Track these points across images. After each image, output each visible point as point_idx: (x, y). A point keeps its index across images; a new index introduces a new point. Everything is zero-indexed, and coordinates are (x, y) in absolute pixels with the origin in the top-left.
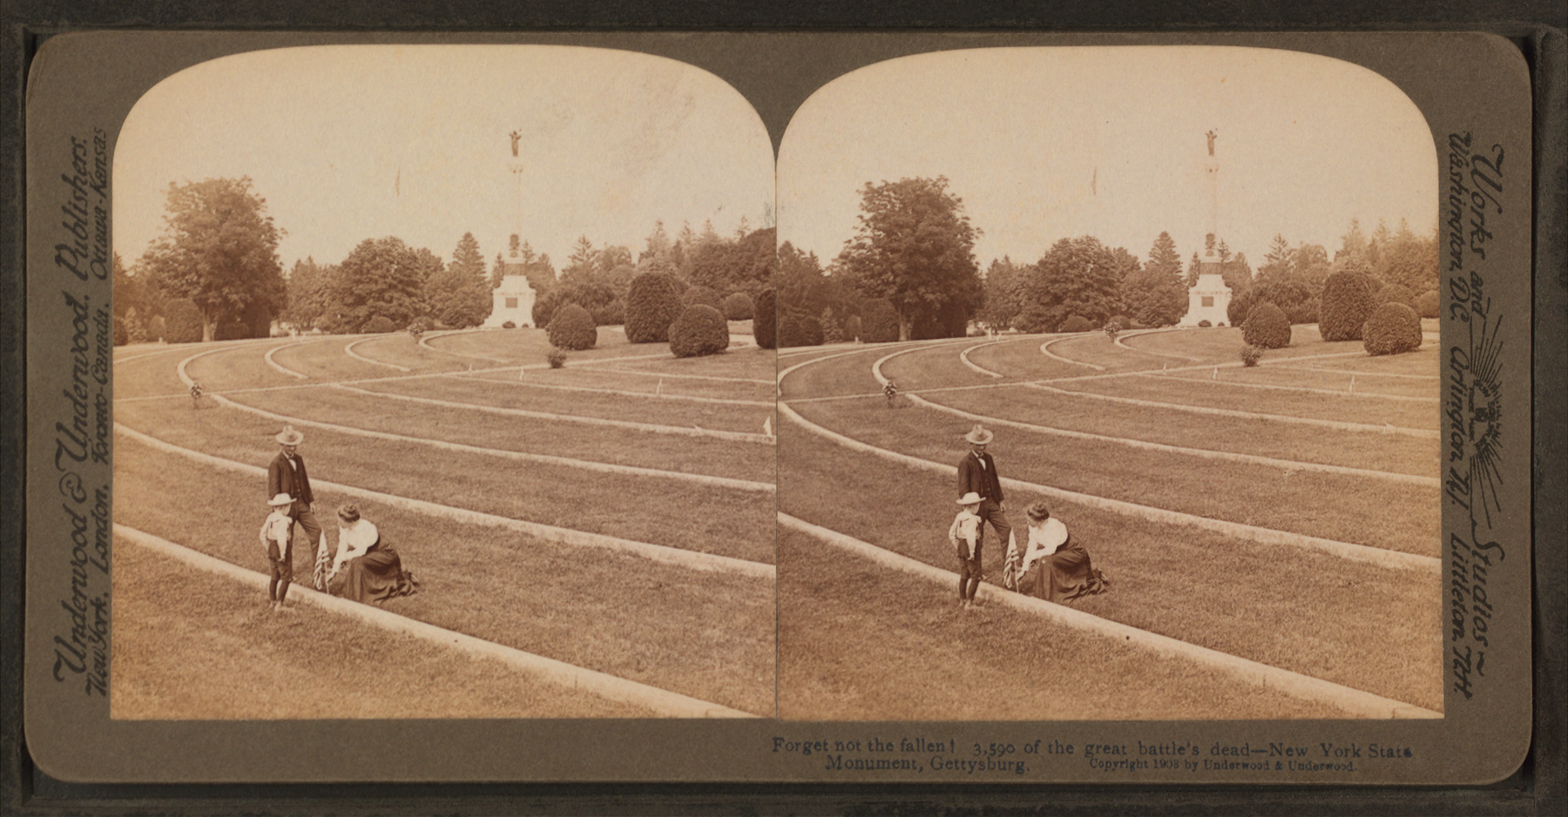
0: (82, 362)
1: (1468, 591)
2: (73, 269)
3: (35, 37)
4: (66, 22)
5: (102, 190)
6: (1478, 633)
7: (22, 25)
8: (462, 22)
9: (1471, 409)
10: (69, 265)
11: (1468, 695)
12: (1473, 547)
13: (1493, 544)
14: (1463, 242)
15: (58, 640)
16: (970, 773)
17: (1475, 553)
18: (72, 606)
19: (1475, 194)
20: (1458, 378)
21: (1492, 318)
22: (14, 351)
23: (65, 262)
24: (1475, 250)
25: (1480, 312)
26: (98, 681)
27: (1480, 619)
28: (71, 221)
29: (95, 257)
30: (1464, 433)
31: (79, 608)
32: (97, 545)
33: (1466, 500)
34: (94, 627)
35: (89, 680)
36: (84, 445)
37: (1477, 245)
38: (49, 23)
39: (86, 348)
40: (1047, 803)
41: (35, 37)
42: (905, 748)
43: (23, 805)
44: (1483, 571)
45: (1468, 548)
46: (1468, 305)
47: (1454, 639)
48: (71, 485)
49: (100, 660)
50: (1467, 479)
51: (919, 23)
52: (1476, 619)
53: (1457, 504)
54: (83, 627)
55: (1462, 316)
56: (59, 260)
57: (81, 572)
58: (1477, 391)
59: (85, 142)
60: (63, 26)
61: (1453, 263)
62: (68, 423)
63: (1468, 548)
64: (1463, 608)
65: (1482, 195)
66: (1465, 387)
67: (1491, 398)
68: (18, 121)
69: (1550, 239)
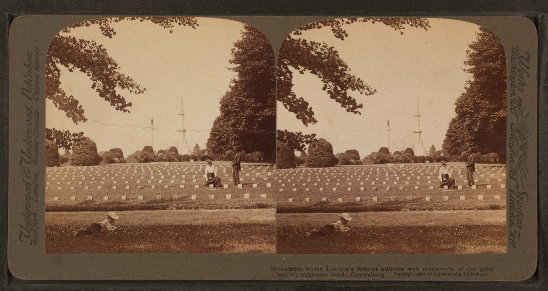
0: (30, 130)
1: (515, 210)
2: (27, 97)
3: (12, 17)
4: (23, 11)
5: (38, 69)
6: (518, 225)
7: (8, 12)
8: (162, 11)
9: (517, 145)
10: (26, 95)
11: (514, 246)
12: (517, 194)
13: (524, 193)
14: (516, 87)
15: (20, 226)
16: (365, 278)
17: (518, 196)
18: (26, 214)
19: (520, 70)
20: (513, 134)
21: (525, 114)
22: (5, 127)
23: (24, 94)
24: (520, 90)
25: (521, 111)
26: (35, 241)
27: (519, 220)
28: (26, 80)
29: (34, 93)
30: (515, 154)
31: (28, 215)
32: (34, 193)
33: (515, 177)
34: (33, 222)
35: (32, 241)
36: (30, 158)
37: (520, 88)
38: (17, 12)
39: (31, 124)
40: (367, 285)
41: (12, 17)
42: (359, 269)
43: (8, 285)
44: (521, 203)
45: (515, 194)
46: (517, 109)
47: (510, 227)
48: (25, 172)
49: (36, 233)
50: (516, 170)
51: (322, 12)
52: (518, 220)
53: (512, 179)
54: (30, 222)
55: (515, 112)
56: (23, 93)
57: (29, 202)
58: (519, 139)
59: (32, 52)
60: (22, 13)
61: (512, 94)
62: (25, 151)
63: (515, 194)
64: (513, 216)
65: (523, 70)
66: (515, 138)
67: (524, 142)
68: (7, 46)
69: (544, 88)
